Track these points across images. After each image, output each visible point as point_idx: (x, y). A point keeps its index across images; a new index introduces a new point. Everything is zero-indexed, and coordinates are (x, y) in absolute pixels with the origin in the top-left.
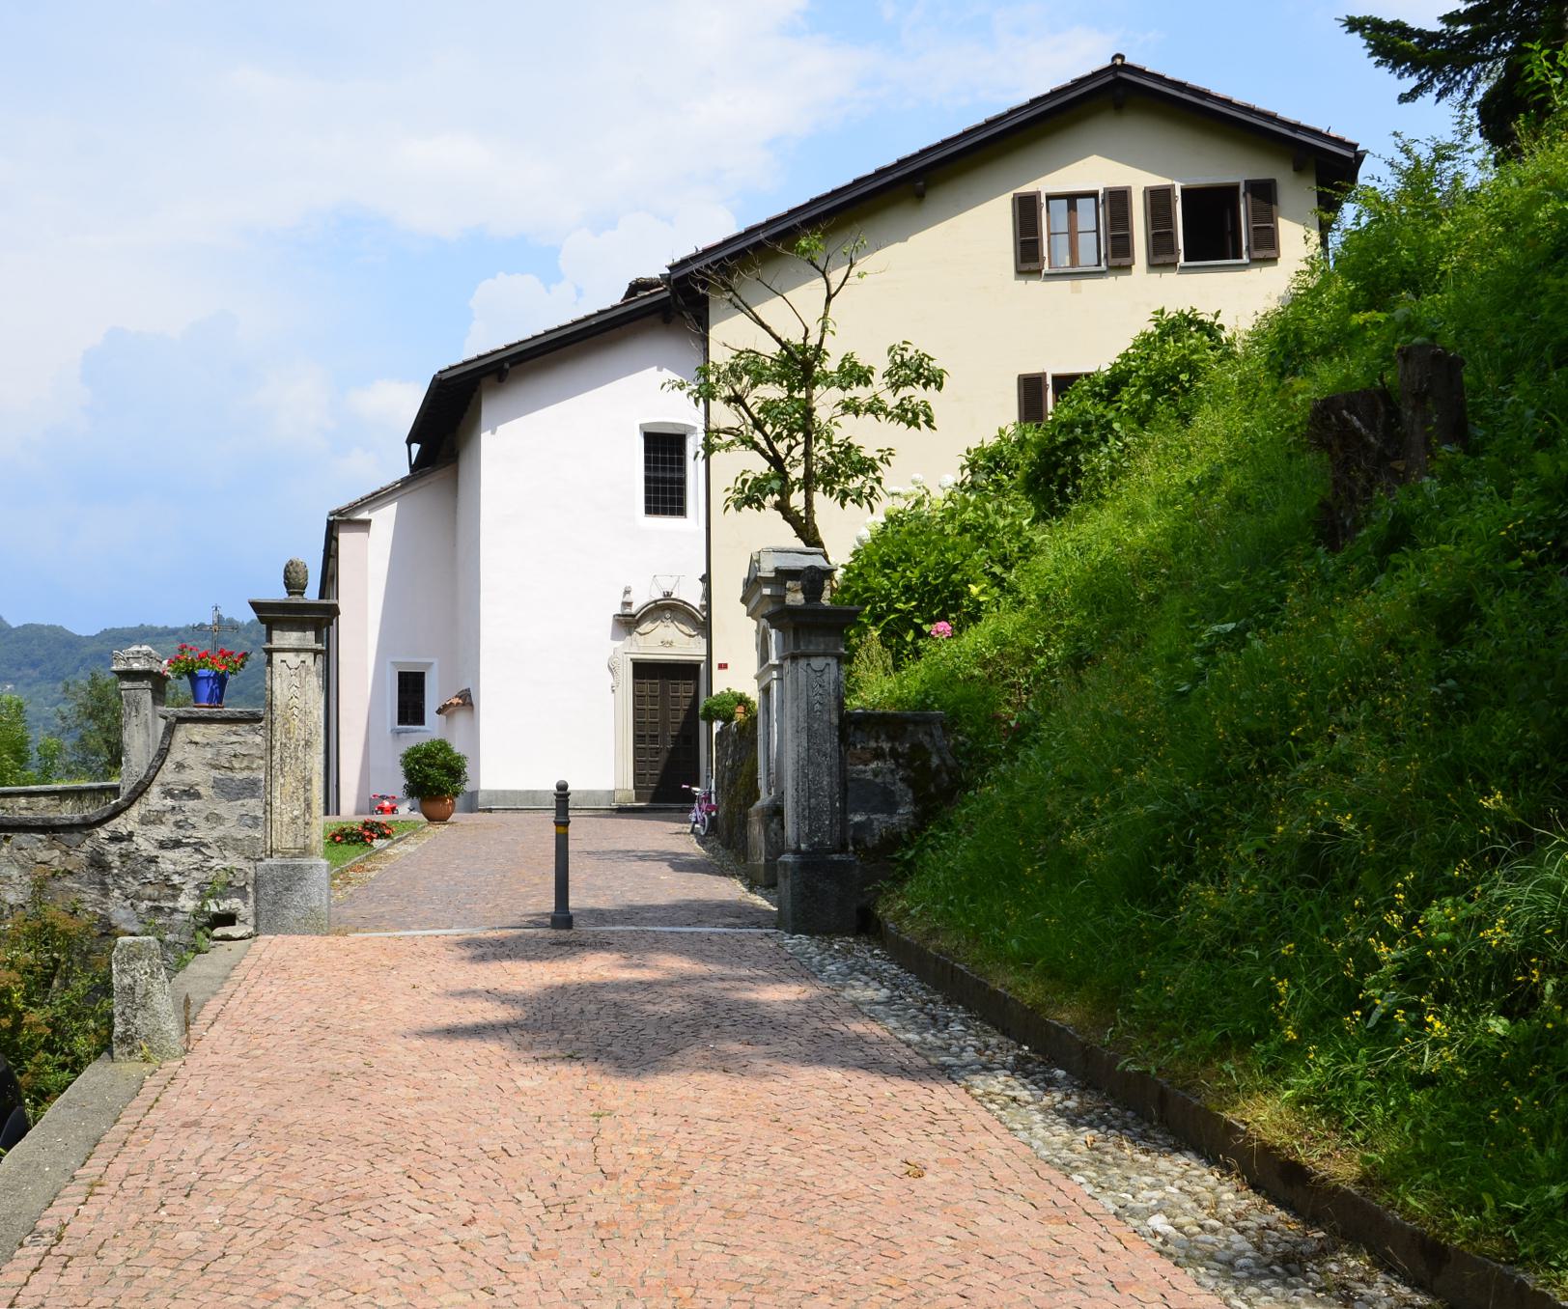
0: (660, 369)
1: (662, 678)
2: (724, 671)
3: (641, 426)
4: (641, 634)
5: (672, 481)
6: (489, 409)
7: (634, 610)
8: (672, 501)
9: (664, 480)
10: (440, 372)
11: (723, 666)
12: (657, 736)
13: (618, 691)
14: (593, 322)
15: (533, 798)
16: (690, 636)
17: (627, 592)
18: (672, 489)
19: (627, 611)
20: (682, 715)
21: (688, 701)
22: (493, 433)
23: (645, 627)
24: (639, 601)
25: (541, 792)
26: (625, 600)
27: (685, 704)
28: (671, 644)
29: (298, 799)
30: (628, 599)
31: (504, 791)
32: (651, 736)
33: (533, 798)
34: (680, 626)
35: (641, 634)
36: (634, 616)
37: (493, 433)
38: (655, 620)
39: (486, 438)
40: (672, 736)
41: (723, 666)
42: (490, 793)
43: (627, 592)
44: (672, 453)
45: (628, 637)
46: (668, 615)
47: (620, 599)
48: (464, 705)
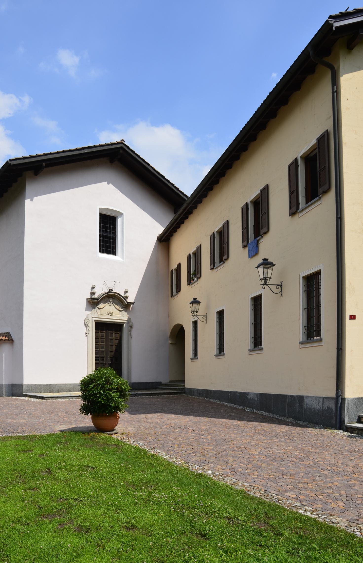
0: (108, 184)
1: (106, 330)
2: (352, 321)
3: (100, 209)
4: (99, 309)
5: (110, 238)
6: (29, 189)
7: (96, 296)
8: (110, 247)
9: (106, 237)
10: (10, 160)
11: (352, 317)
12: (104, 358)
13: (89, 335)
14: (86, 151)
15: (50, 388)
16: (120, 311)
17: (93, 288)
18: (110, 242)
19: (93, 297)
20: (114, 348)
21: (117, 341)
22: (32, 200)
23: (101, 305)
24: (99, 292)
25: (53, 385)
26: (93, 291)
27: (116, 343)
28: (112, 314)
29: (54, 427)
30: (94, 291)
31: (36, 385)
32: (101, 357)
33: (50, 388)
34: (116, 306)
35: (99, 309)
36: (97, 299)
37: (32, 200)
38: (105, 302)
39: (28, 202)
40: (110, 358)
41: (352, 317)
42: (28, 386)
43: (93, 288)
44: (110, 224)
45: (93, 310)
46: (111, 300)
47: (89, 291)
48: (9, 340)
